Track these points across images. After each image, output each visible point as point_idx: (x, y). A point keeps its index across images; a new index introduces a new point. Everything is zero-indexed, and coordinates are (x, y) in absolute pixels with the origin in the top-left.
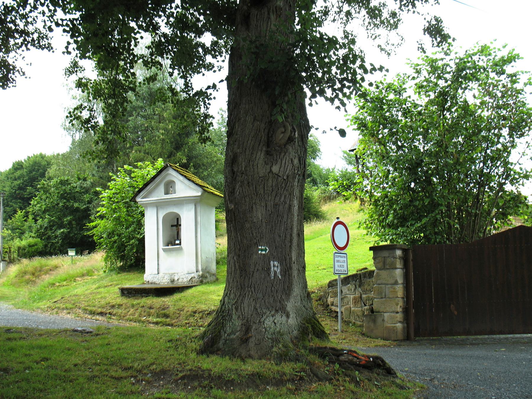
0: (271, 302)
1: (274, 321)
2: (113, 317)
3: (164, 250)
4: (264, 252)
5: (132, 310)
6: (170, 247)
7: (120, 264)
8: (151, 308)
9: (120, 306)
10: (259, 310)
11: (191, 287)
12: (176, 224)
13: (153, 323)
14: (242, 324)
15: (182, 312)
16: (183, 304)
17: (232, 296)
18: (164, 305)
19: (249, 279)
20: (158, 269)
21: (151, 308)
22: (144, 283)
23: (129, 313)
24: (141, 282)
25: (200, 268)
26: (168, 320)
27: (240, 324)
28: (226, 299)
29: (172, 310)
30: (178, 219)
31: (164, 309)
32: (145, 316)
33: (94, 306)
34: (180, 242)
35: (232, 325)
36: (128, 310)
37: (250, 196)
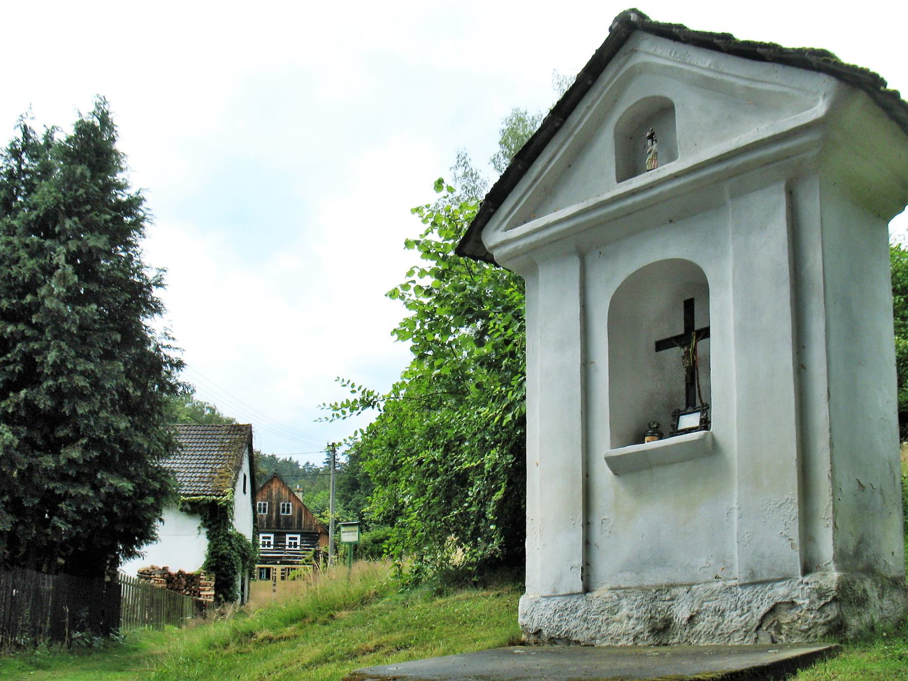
3: (617, 465)
25: (826, 548)
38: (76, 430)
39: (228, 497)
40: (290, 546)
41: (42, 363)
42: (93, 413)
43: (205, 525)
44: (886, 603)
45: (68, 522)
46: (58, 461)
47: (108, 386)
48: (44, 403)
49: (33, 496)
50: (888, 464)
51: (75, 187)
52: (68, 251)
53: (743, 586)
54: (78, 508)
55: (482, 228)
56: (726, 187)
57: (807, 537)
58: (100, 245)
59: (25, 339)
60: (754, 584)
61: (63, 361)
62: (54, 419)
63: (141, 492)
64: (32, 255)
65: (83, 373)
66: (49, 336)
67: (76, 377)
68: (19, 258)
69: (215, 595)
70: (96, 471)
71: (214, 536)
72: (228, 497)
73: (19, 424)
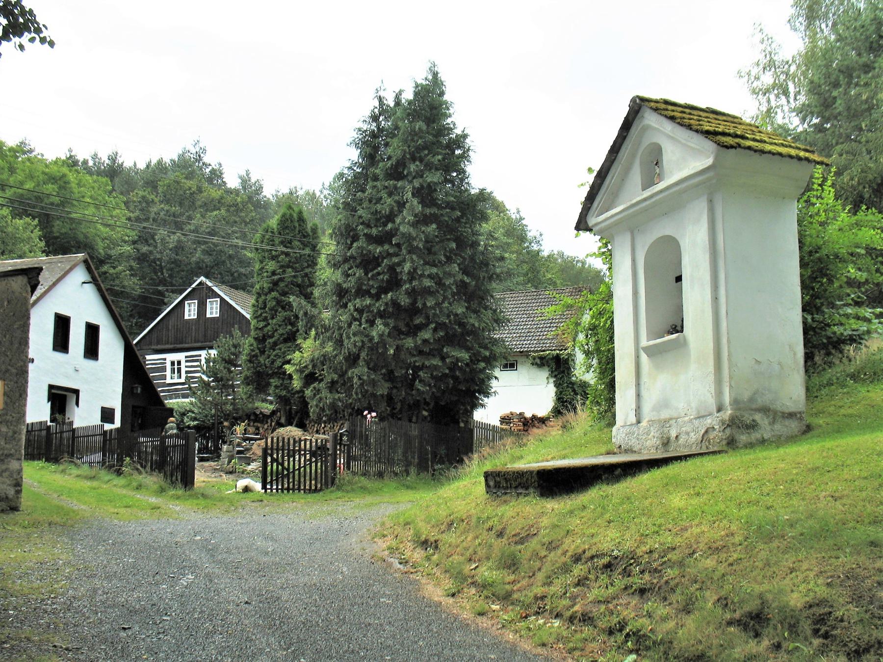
3: (649, 351)
25: (727, 399)
38: (427, 317)
39: (569, 351)
41: (401, 272)
42: (438, 304)
43: (551, 376)
45: (425, 385)
46: (416, 342)
47: (448, 283)
48: (404, 301)
49: (401, 368)
50: (787, 347)
51: (416, 138)
52: (414, 188)
53: (696, 418)
54: (432, 375)
55: (586, 215)
57: (719, 393)
58: (435, 180)
59: (389, 255)
60: (699, 417)
61: (415, 269)
62: (413, 311)
63: (476, 358)
64: (390, 194)
65: (430, 276)
66: (404, 251)
67: (425, 280)
68: (381, 198)
70: (443, 347)
71: (560, 384)
72: (569, 351)
73: (389, 318)
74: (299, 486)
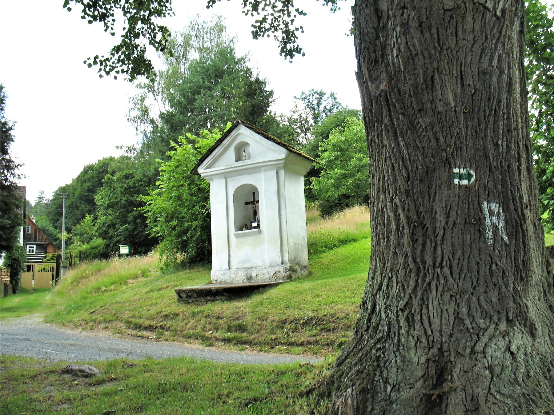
0: (494, 300)
1: (508, 348)
2: (166, 333)
3: (237, 236)
4: (465, 182)
5: (193, 321)
6: (245, 231)
7: (180, 257)
8: (218, 318)
9: (176, 315)
10: (467, 322)
11: (276, 285)
12: (252, 200)
13: (223, 340)
14: (428, 360)
15: (264, 323)
16: (266, 310)
17: (394, 291)
18: (238, 313)
19: (435, 248)
20: (229, 261)
21: (218, 318)
22: (210, 283)
23: (188, 326)
24: (207, 282)
25: (286, 258)
26: (244, 334)
27: (423, 359)
28: (380, 297)
29: (249, 319)
30: (254, 194)
31: (238, 319)
32: (211, 330)
33: (141, 318)
34: (259, 225)
35: (403, 362)
36: (186, 321)
37: (426, 54)
40: (29, 251)
44: (302, 272)
56: (263, 168)
57: (282, 256)
69: (10, 281)
74: (441, 264)
